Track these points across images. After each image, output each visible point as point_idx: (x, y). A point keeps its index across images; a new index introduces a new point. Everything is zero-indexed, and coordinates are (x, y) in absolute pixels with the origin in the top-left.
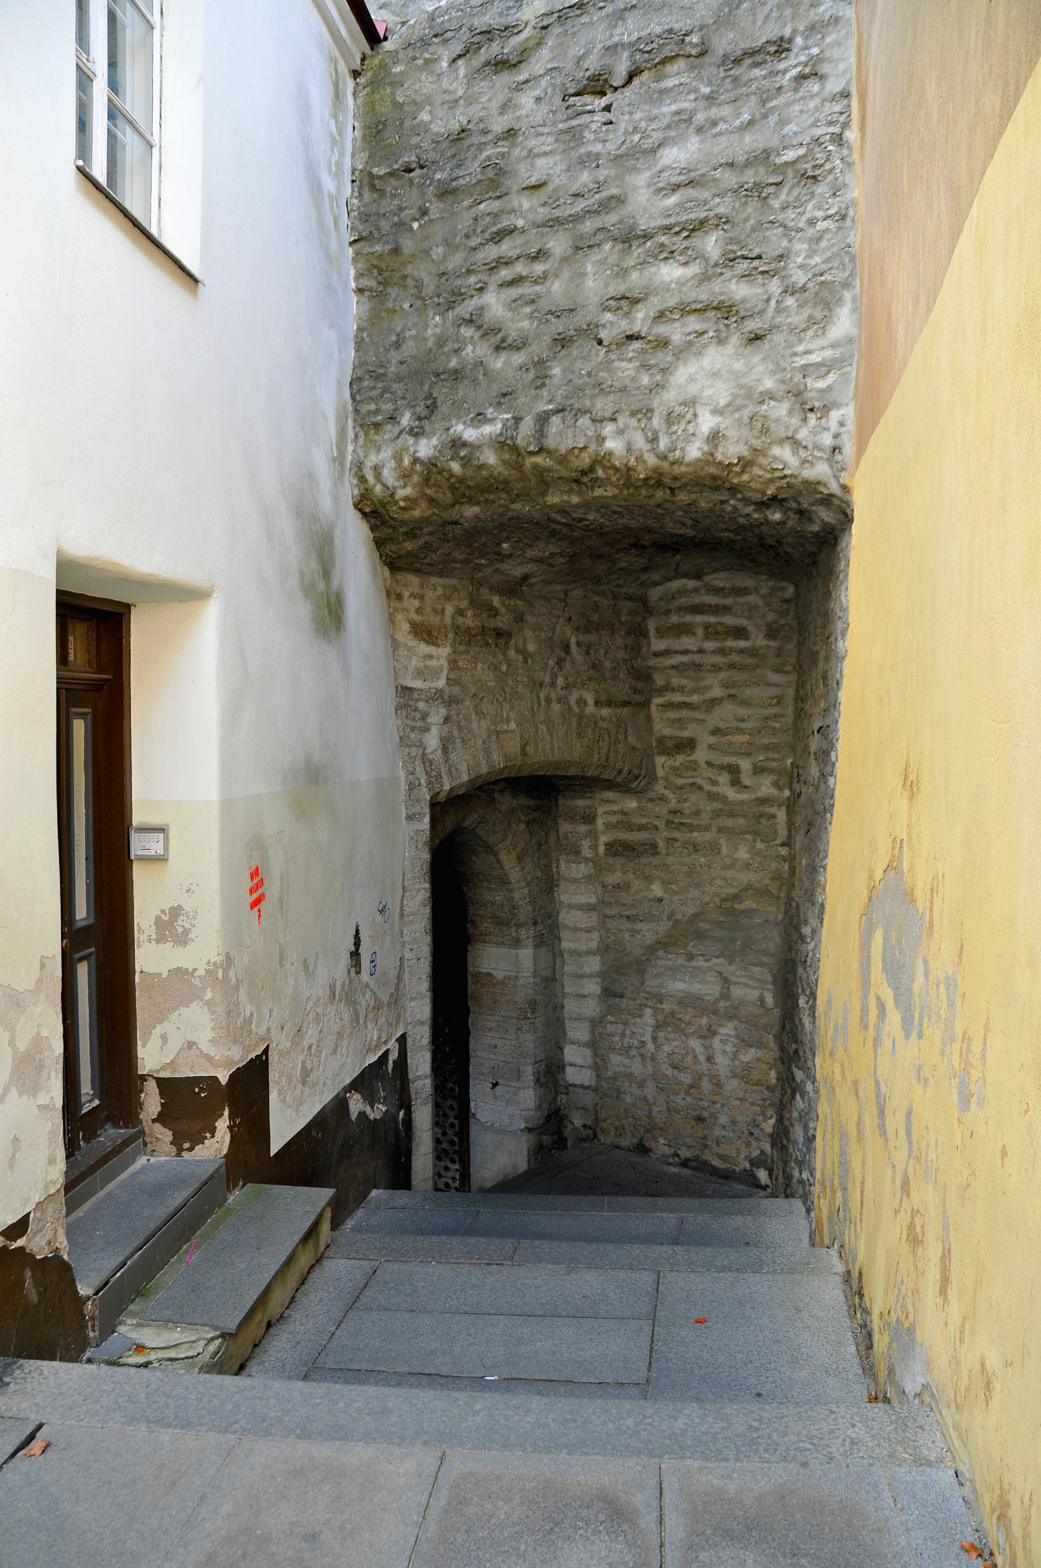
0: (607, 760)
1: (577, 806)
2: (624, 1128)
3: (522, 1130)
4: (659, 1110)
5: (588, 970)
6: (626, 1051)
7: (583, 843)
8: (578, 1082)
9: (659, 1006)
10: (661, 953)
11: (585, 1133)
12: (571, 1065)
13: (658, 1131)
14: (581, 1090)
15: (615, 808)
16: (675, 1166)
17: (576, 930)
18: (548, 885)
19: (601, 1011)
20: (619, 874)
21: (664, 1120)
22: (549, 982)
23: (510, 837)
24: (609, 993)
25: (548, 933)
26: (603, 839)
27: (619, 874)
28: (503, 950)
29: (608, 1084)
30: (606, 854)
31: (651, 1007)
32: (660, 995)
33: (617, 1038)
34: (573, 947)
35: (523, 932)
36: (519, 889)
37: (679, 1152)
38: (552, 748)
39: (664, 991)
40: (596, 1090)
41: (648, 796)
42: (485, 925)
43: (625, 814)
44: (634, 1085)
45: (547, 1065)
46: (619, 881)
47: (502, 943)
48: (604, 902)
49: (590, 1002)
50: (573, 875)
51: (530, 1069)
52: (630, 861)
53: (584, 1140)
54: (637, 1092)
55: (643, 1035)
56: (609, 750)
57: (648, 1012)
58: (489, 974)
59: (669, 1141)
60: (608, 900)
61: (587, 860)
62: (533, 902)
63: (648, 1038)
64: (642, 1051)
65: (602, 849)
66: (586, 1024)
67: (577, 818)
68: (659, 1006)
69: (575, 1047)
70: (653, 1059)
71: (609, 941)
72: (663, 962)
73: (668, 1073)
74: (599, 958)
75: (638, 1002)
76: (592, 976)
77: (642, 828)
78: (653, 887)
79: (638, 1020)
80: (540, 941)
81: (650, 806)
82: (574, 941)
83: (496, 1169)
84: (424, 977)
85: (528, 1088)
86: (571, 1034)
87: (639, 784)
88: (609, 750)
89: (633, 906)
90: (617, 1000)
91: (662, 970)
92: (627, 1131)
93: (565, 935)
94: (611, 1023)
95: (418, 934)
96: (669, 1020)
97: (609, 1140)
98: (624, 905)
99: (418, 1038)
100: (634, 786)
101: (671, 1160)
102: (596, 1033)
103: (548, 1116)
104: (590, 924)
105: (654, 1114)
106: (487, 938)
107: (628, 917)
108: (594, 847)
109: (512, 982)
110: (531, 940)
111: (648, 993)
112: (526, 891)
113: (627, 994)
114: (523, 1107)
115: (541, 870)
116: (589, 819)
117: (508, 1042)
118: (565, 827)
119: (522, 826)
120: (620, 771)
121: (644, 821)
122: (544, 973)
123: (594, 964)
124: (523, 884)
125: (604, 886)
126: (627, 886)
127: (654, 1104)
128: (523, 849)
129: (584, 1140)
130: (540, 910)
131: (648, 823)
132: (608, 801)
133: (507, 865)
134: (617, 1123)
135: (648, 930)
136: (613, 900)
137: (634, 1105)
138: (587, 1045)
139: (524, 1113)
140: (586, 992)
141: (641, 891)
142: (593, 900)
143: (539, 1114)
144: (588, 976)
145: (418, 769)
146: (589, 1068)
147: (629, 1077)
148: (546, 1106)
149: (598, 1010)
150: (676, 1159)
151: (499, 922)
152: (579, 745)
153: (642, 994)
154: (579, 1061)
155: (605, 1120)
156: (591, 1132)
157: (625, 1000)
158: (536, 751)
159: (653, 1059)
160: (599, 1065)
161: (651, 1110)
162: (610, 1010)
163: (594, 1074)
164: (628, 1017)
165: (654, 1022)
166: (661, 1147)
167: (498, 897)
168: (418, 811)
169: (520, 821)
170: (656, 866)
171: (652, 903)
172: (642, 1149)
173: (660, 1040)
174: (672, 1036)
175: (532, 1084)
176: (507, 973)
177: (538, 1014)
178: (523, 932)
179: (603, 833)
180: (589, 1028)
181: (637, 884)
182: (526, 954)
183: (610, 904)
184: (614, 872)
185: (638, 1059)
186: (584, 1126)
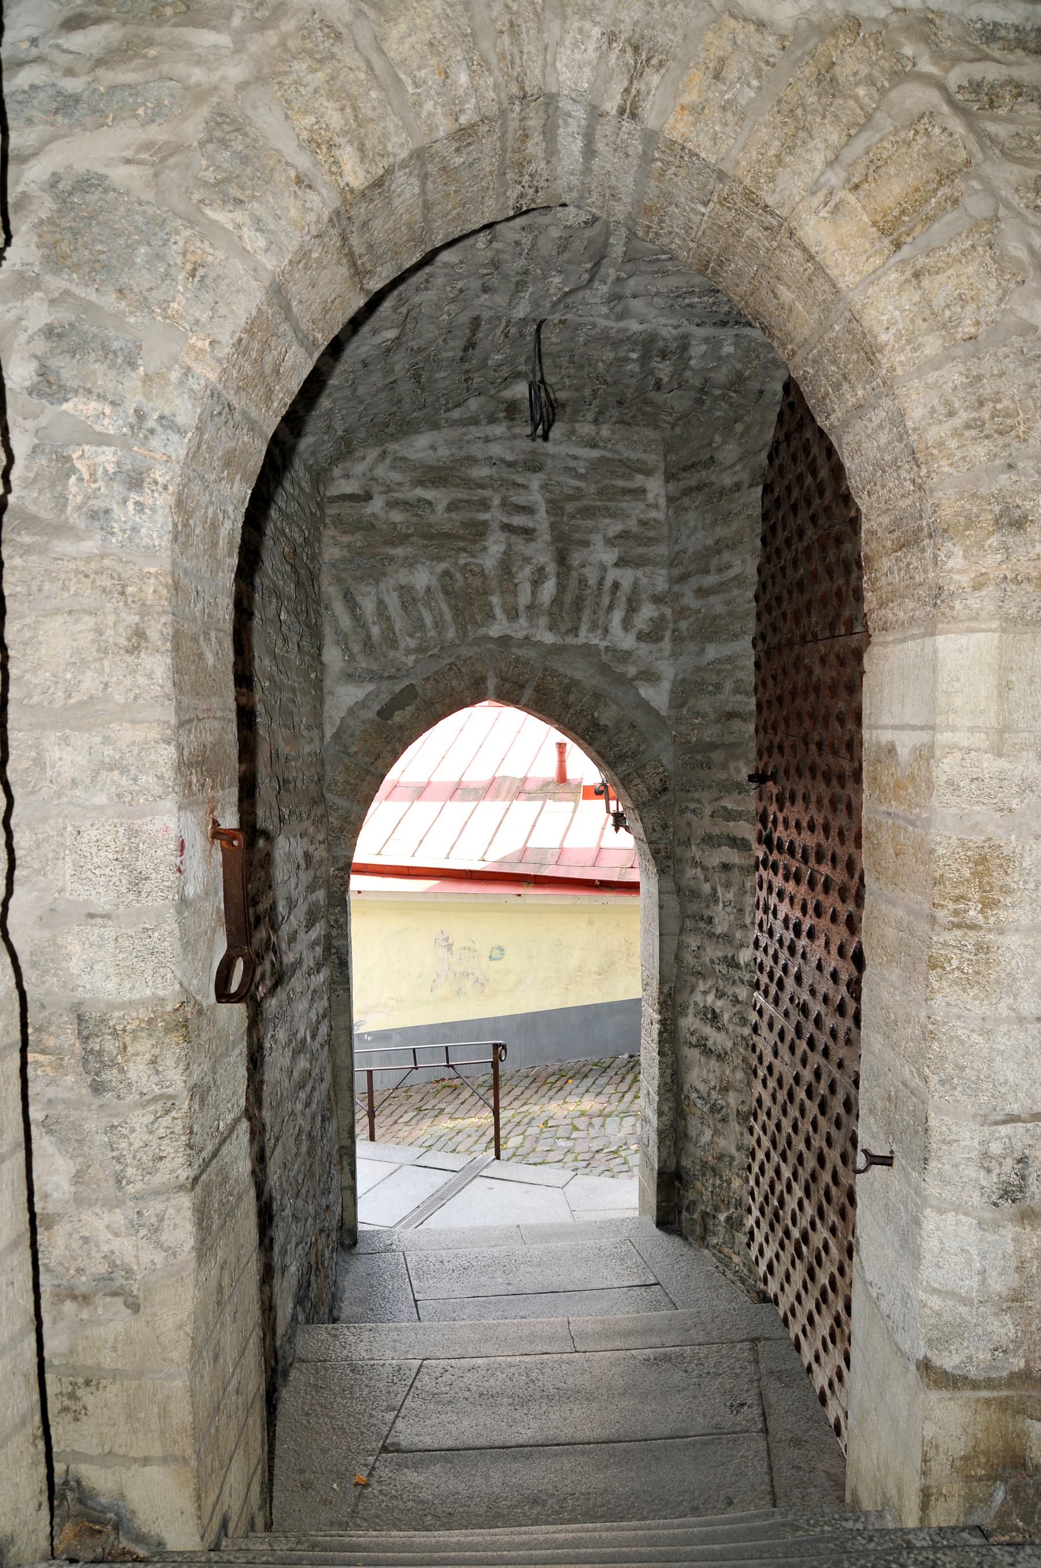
36: (920, 372)
112: (954, 375)
128: (919, 197)
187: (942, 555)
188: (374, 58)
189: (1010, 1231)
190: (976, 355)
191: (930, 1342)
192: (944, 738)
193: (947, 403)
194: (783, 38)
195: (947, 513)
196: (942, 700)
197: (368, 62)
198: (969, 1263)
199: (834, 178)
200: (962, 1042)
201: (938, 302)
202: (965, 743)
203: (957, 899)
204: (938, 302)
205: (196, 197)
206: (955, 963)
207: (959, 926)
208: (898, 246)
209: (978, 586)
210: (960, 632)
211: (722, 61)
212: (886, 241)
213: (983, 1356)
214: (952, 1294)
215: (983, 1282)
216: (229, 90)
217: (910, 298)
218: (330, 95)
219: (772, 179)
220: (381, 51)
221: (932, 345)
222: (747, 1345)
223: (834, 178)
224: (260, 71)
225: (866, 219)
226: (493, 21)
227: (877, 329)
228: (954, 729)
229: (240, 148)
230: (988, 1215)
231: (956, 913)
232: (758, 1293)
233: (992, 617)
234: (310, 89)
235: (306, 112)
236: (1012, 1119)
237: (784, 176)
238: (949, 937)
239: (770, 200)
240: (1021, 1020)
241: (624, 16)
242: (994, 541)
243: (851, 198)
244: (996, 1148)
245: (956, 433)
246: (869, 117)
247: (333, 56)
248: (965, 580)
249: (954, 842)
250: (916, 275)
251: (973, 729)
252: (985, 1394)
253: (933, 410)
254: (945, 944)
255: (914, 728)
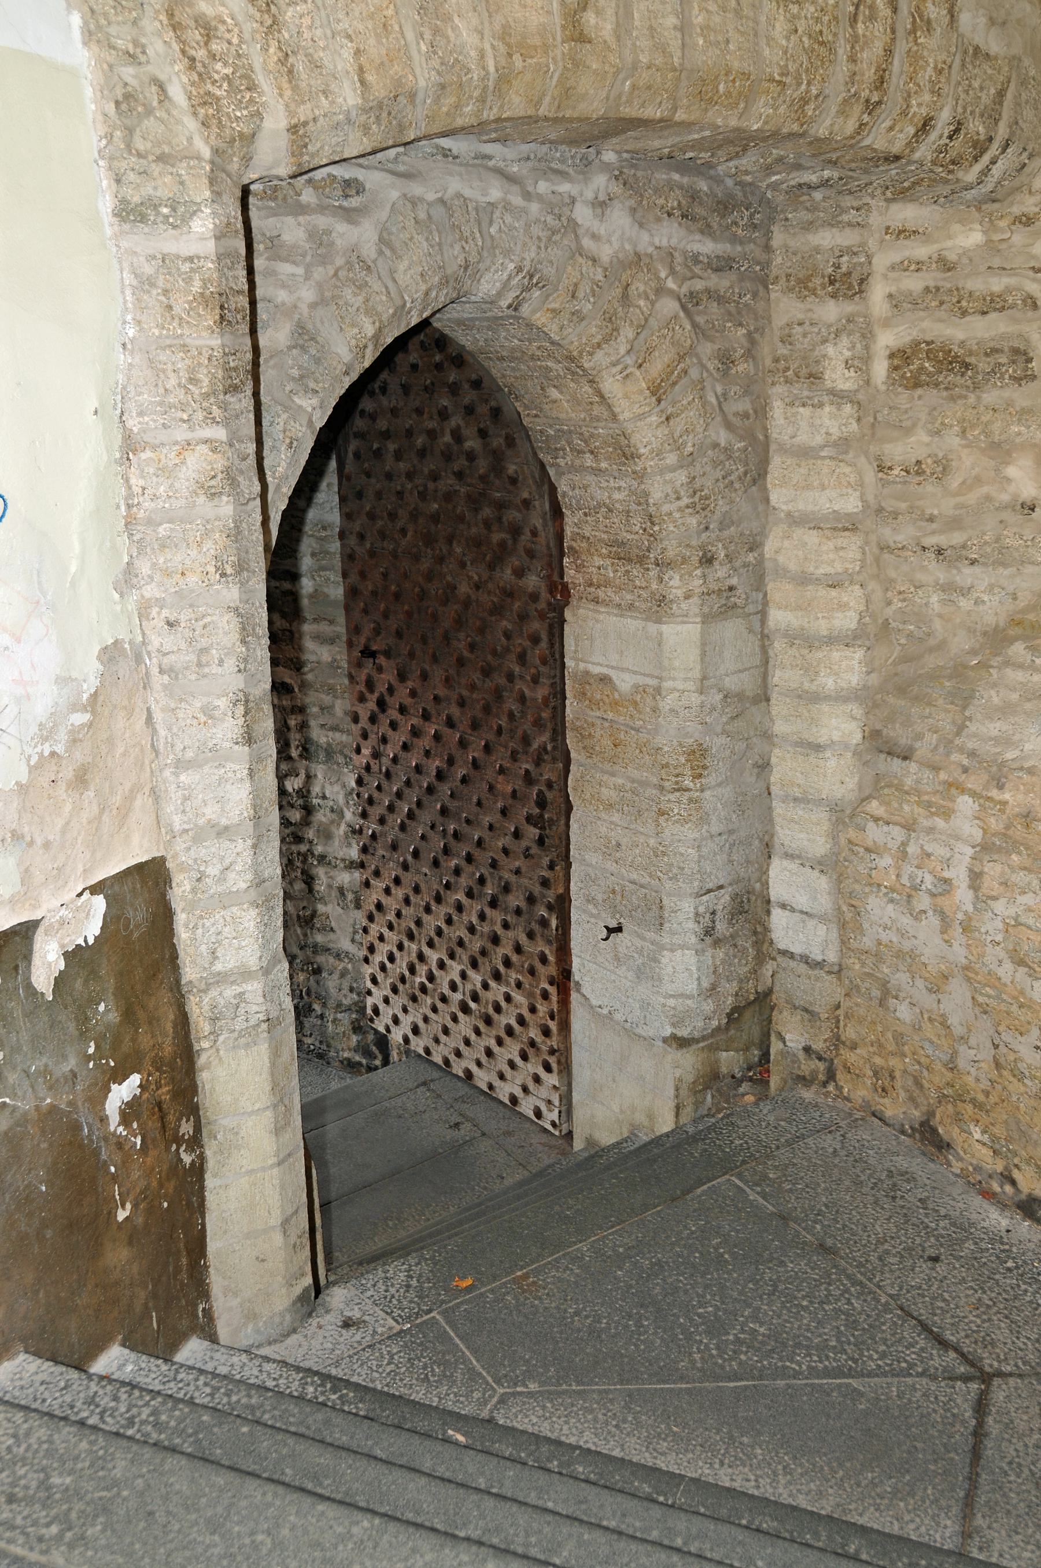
0: (880, 83)
1: (817, 250)
2: (892, 1078)
3: (665, 1040)
4: (975, 1062)
5: (830, 683)
6: (906, 896)
7: (830, 350)
8: (797, 949)
9: (994, 793)
10: (1018, 649)
11: (808, 1066)
12: (783, 906)
13: (969, 1108)
14: (803, 968)
15: (921, 251)
16: (1003, 1206)
17: (804, 580)
18: (752, 462)
19: (860, 786)
20: (921, 436)
21: (985, 1084)
22: (750, 702)
23: (627, 332)
24: (881, 745)
25: (739, 594)
26: (887, 340)
27: (921, 436)
28: (632, 624)
29: (863, 964)
30: (890, 381)
31: (974, 794)
32: (1003, 764)
33: (886, 861)
34: (796, 623)
35: (676, 582)
36: (662, 472)
37: (1016, 1174)
38: (684, 28)
39: (1010, 755)
40: (838, 971)
41: (1016, 210)
42: (598, 561)
43: (946, 266)
44: (920, 983)
45: (735, 897)
46: (921, 453)
47: (631, 606)
48: (880, 510)
49: (832, 763)
50: (803, 438)
51: (688, 906)
52: (953, 399)
53: (805, 1081)
54: (928, 1001)
55: (948, 862)
56: (889, 52)
57: (965, 804)
58: (605, 680)
59: (994, 1138)
60: (889, 504)
61: (838, 396)
62: (701, 505)
63: (959, 874)
64: (944, 902)
65: (880, 369)
66: (821, 817)
67: (817, 281)
68: (994, 793)
69: (793, 866)
70: (967, 928)
71: (889, 612)
72: (1019, 676)
73: (1001, 972)
74: (859, 654)
75: (943, 776)
76: (842, 697)
77: (993, 304)
78: (1012, 471)
79: (940, 823)
80: (722, 604)
81: (1019, 238)
82: (798, 608)
83: (616, 1108)
84: (223, 703)
85: (683, 947)
86: (786, 835)
87: (986, 172)
88: (889, 52)
89: (955, 523)
90: (896, 764)
91: (1014, 697)
92: (898, 1084)
93: (778, 590)
94: (876, 820)
95: (193, 579)
96: (1019, 832)
97: (861, 1093)
98: (931, 519)
99: (213, 870)
100: (970, 176)
101: (996, 1187)
102: (843, 841)
103: (735, 1009)
104: (839, 567)
105: (961, 1063)
106: (601, 593)
107: (940, 552)
108: (860, 363)
109: (649, 700)
110: (695, 600)
111: (972, 754)
112: (681, 477)
113: (922, 750)
114: (669, 988)
115: (729, 426)
116: (847, 282)
117: (642, 839)
118: (785, 307)
119: (669, 306)
120: (926, 126)
121: (997, 284)
122: (732, 683)
123: (847, 669)
124: (671, 459)
125: (881, 468)
126: (944, 467)
127: (963, 1039)
128: (670, 369)
129: (805, 1081)
130: (722, 526)
131: (1008, 290)
132: (903, 233)
133: (625, 411)
134: (878, 1061)
135: (990, 589)
136: (903, 506)
137: (917, 1028)
138: (821, 865)
139: (671, 1002)
140: (823, 736)
141: (978, 480)
142: (851, 504)
143: (708, 1006)
144: (827, 698)
145: (156, 47)
146: (823, 919)
147: (908, 958)
148: (729, 988)
149: (852, 783)
150: (1008, 1188)
151: (625, 555)
152: (781, 27)
153: (955, 757)
154: (802, 901)
155: (854, 1047)
156: (821, 1066)
157: (913, 767)
158: (622, 30)
159: (967, 928)
160: (847, 921)
161: (955, 1054)
162: (877, 786)
163: (834, 934)
164: (918, 810)
165: (978, 835)
166: (974, 1144)
167: (614, 490)
168: (164, 193)
169: (660, 291)
170: (1023, 411)
171: (1006, 515)
172: (930, 1138)
173: (990, 884)
174: (1020, 878)
175: (693, 939)
176: (641, 680)
177: (711, 780)
178: (676, 582)
179: (886, 323)
180: (826, 826)
181: (968, 462)
182: (681, 636)
183: (895, 515)
184: (908, 431)
185: (935, 921)
186: (807, 1050)
187: (666, 578)
188: (390, 285)
189: (709, 952)
190: (692, 464)
191: (673, 1025)
192: (668, 684)
193: (676, 492)
194: (606, 269)
195: (670, 554)
196: (666, 663)
197: (387, 288)
198: (691, 976)
199: (629, 360)
200: (682, 855)
201: (677, 434)
202: (681, 687)
203: (677, 776)
204: (677, 434)
205: (288, 388)
206: (676, 811)
207: (678, 790)
208: (659, 401)
209: (687, 597)
210: (678, 623)
211: (576, 285)
212: (654, 399)
213: (700, 1024)
214: (682, 995)
215: (699, 984)
216: (304, 309)
217: (662, 432)
218: (367, 312)
219: (591, 354)
220: (395, 281)
221: (671, 459)
222: (422, 1089)
223: (629, 360)
224: (322, 295)
225: (644, 385)
226: (456, 258)
227: (639, 445)
228: (674, 679)
229: (314, 352)
230: (699, 947)
231: (677, 783)
232: (342, 1062)
233: (696, 615)
234: (355, 308)
235: (353, 325)
236: (709, 891)
237: (599, 355)
238: (672, 797)
239: (586, 365)
240: (712, 836)
241: (526, 255)
242: (698, 572)
243: (638, 373)
244: (701, 909)
245: (680, 510)
246: (646, 320)
247: (366, 283)
248: (679, 593)
249: (675, 743)
250: (668, 419)
251: (685, 680)
252: (701, 1045)
253: (667, 495)
254: (669, 801)
255: (635, 673)
